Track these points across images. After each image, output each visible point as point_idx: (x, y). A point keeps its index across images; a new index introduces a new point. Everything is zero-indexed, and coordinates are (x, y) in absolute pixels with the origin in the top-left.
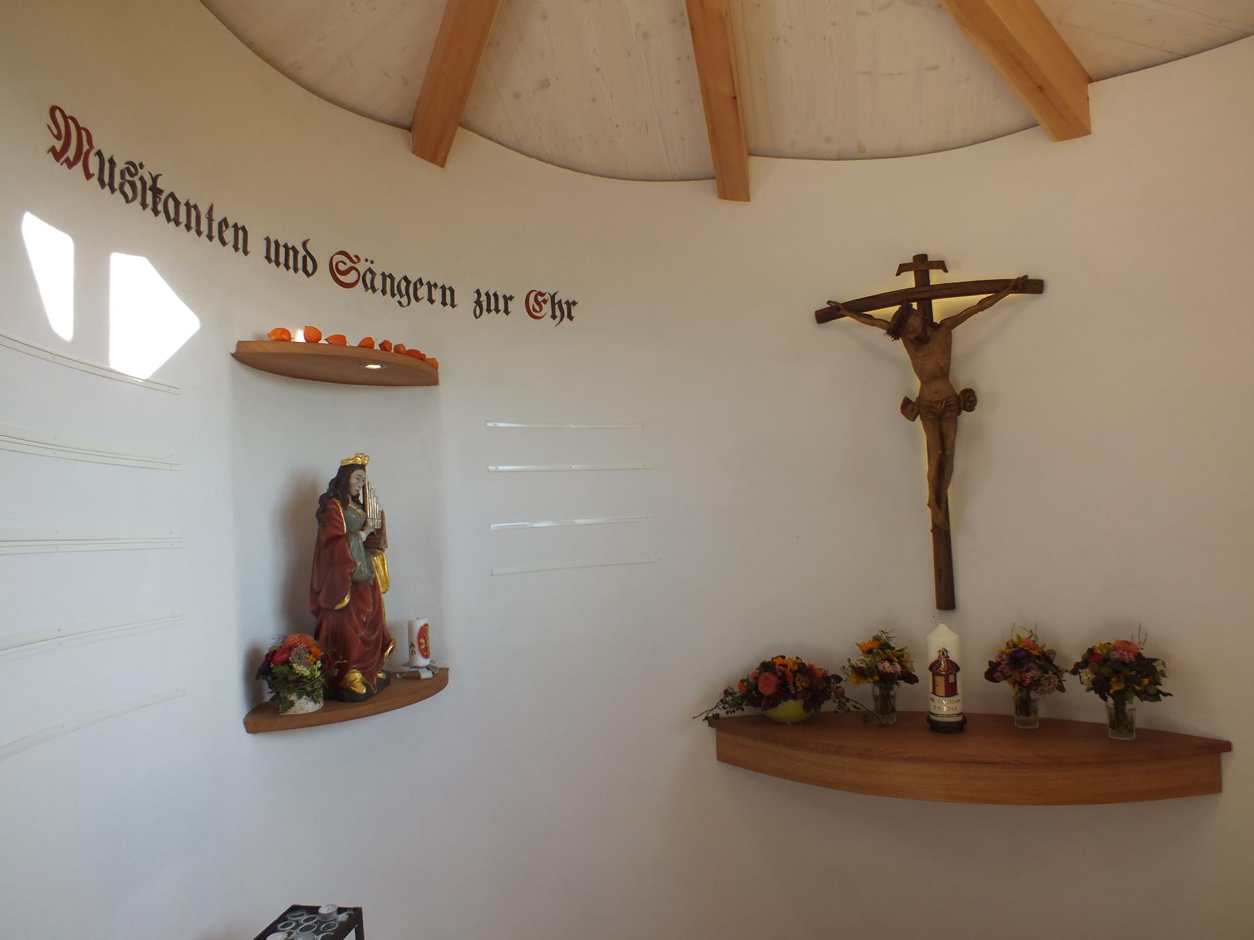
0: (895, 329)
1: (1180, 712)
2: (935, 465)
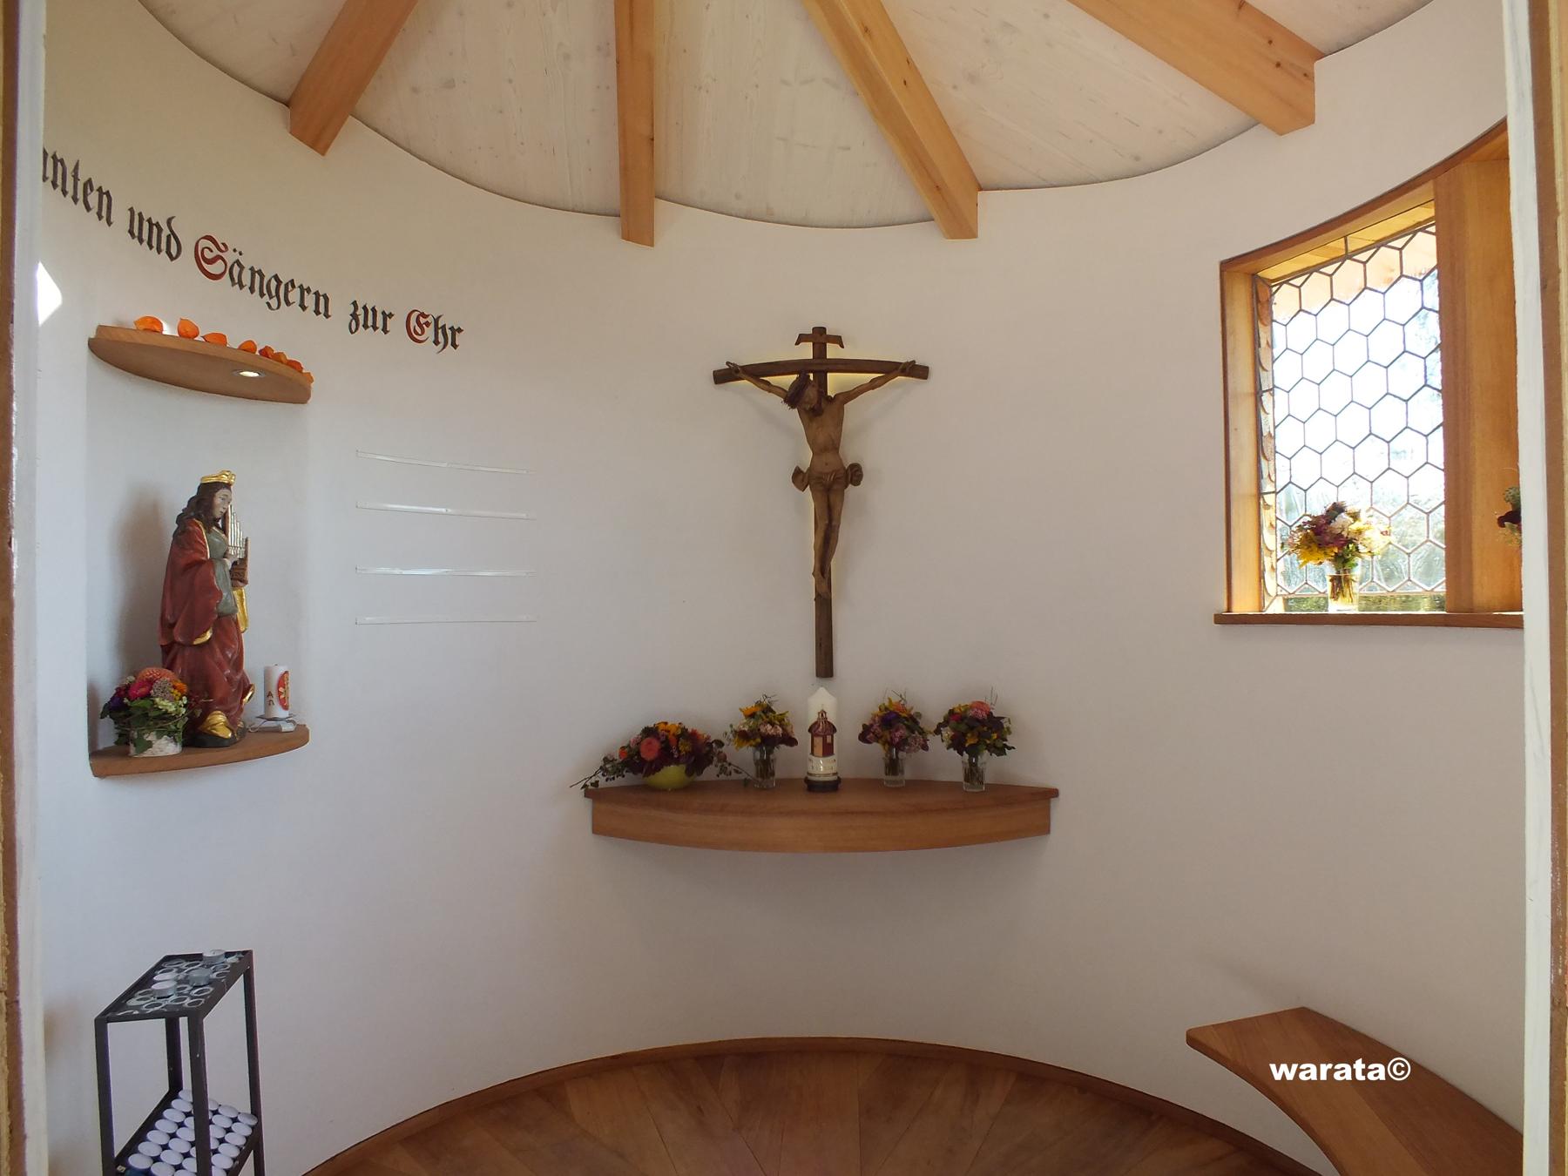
0: (793, 398)
1: (1018, 766)
2: (820, 541)
